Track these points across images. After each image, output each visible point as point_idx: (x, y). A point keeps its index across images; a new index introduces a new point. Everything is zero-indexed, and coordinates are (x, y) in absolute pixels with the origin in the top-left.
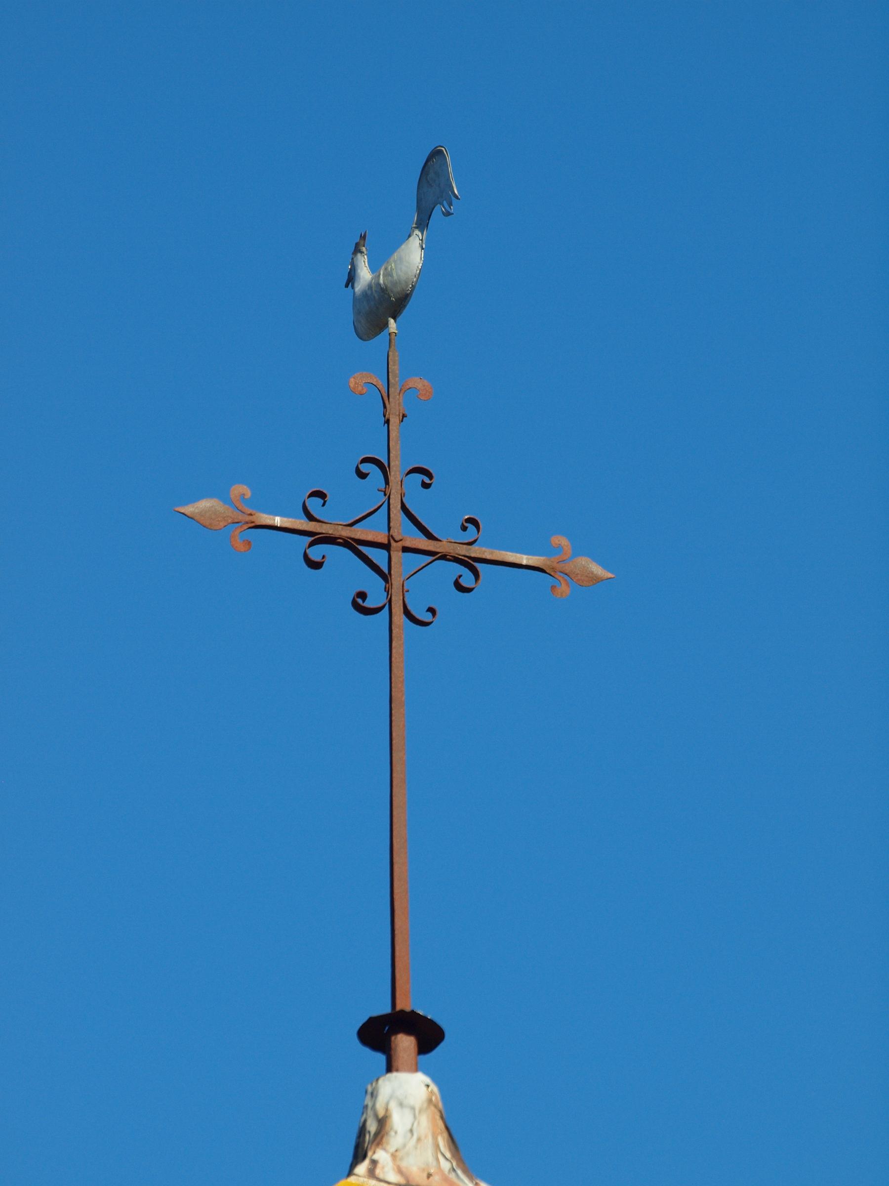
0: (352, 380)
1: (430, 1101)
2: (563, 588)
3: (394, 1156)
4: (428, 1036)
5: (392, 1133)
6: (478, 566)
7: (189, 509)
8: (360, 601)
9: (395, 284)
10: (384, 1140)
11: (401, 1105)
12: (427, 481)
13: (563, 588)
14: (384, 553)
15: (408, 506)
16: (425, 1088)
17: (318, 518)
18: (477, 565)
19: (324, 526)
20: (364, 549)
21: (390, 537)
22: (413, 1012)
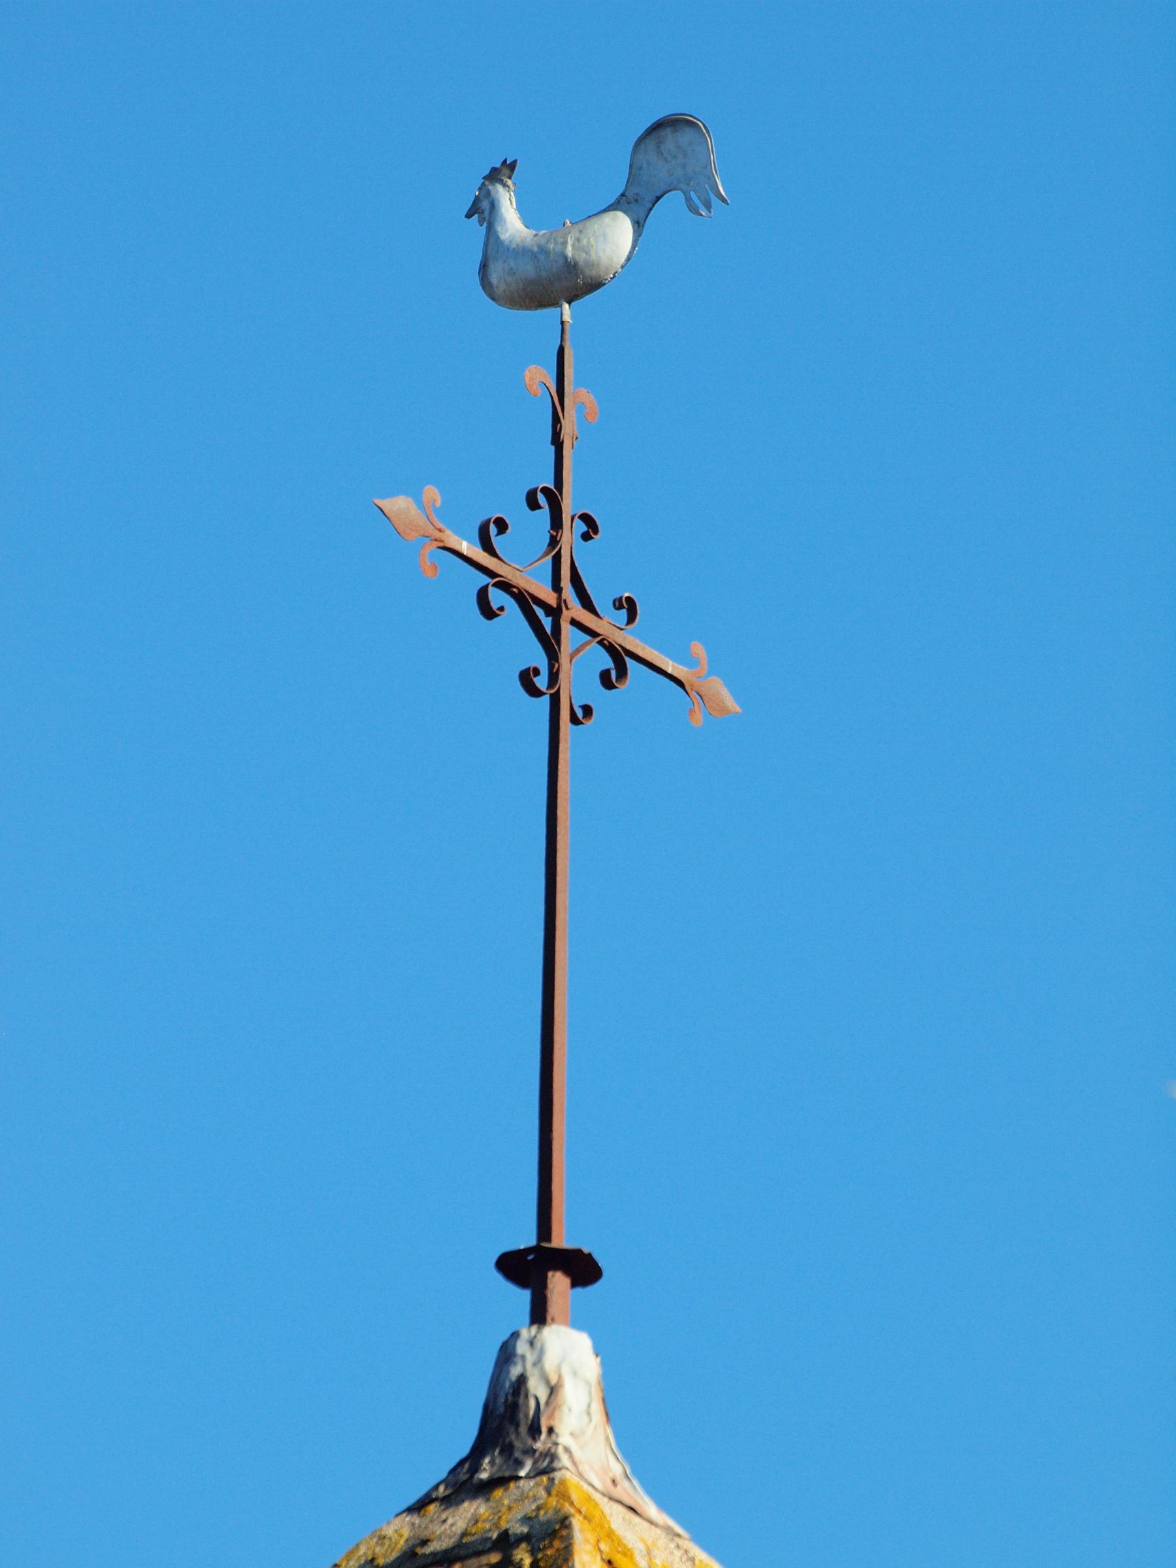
0: (527, 373)
2: (700, 718)
4: (583, 1269)
5: (565, 1409)
6: (629, 662)
9: (592, 265)
13: (700, 718)
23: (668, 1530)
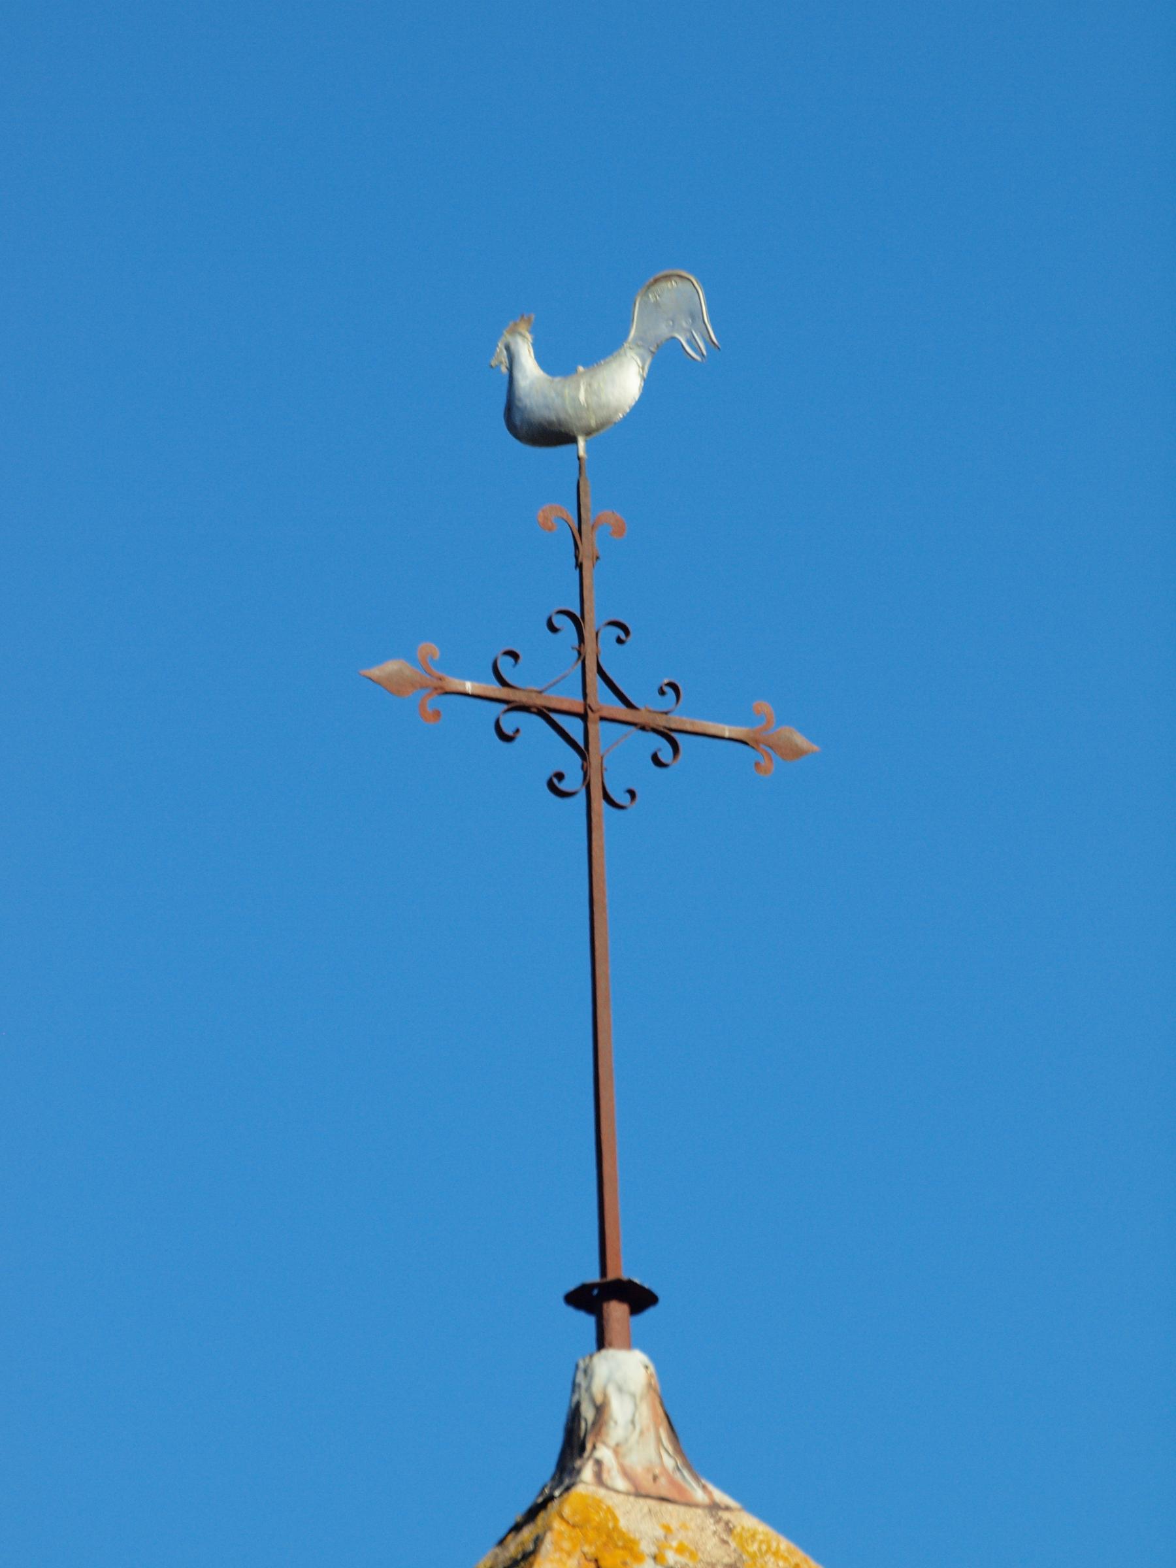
1: (650, 1385)
3: (616, 1451)
4: (639, 1299)
5: (612, 1424)
6: (675, 735)
7: (375, 672)
8: (555, 781)
10: (604, 1429)
11: (620, 1390)
12: (623, 636)
14: (579, 723)
15: (605, 668)
16: (643, 1370)
19: (517, 692)
20: (556, 717)
21: (587, 706)
22: (630, 1282)
23: (714, 1507)
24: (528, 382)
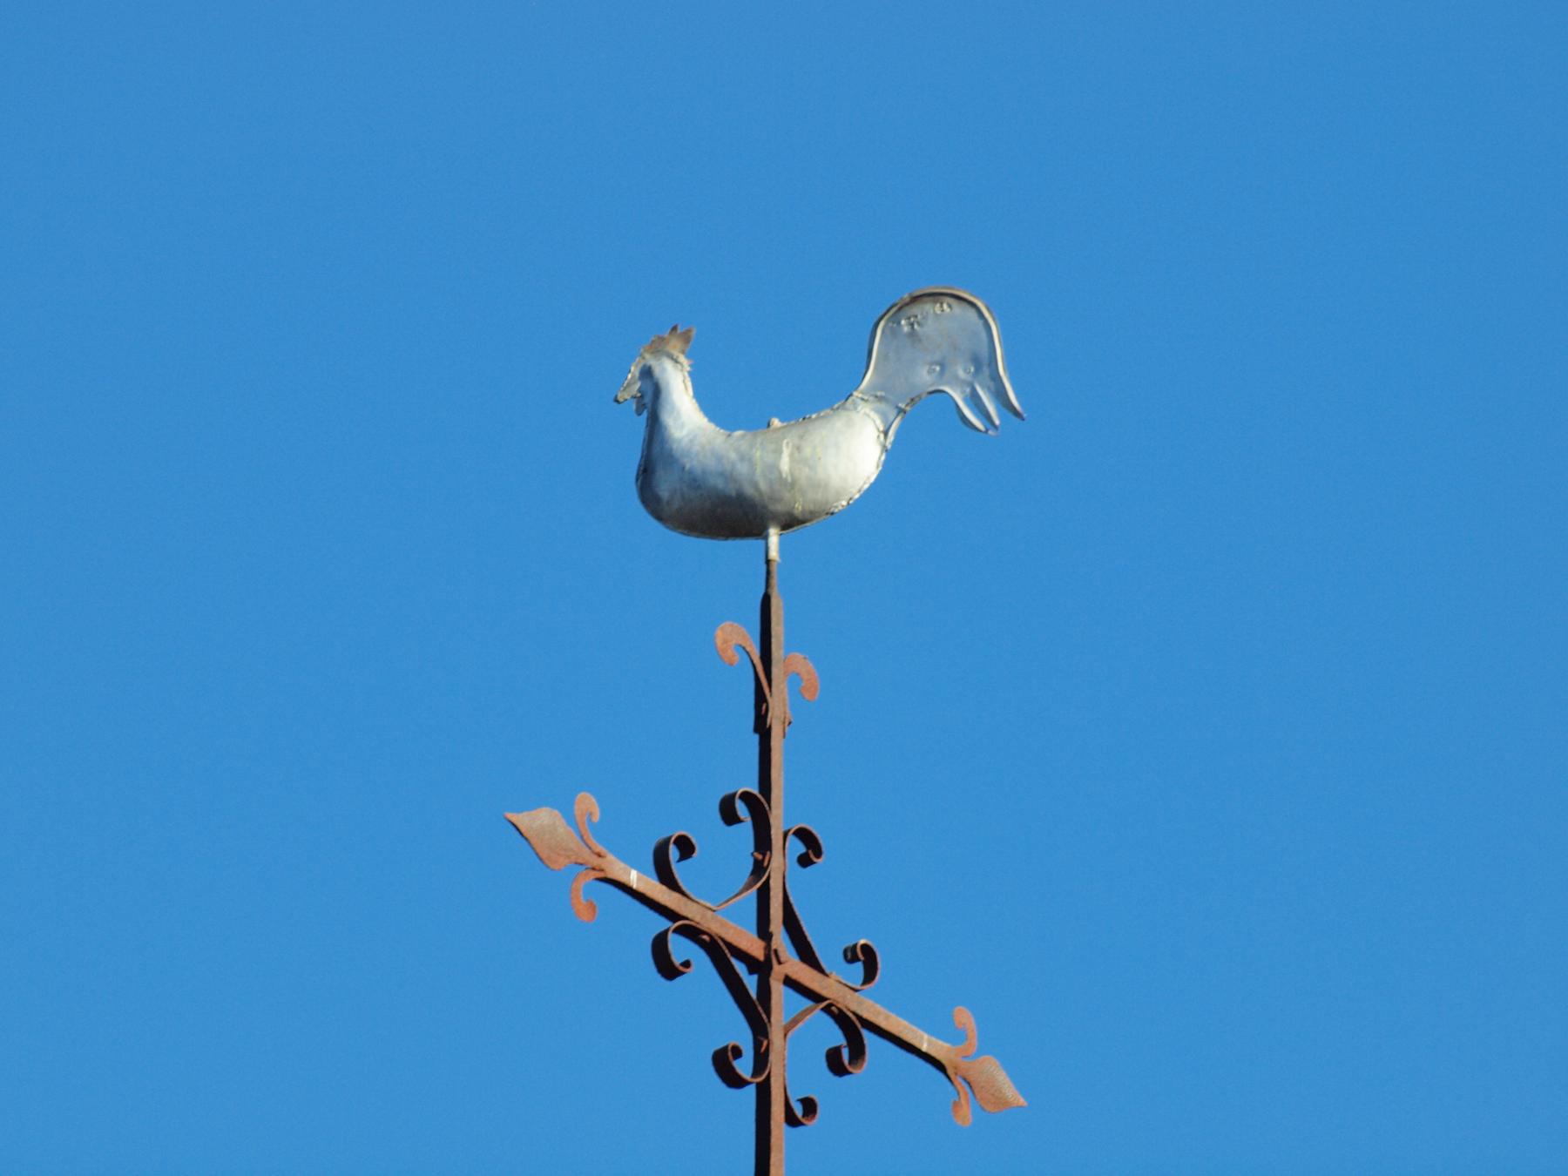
2: (968, 1112)
6: (867, 1036)
13: (968, 1112)
17: (684, 888)
18: (866, 1034)
24: (685, 432)
